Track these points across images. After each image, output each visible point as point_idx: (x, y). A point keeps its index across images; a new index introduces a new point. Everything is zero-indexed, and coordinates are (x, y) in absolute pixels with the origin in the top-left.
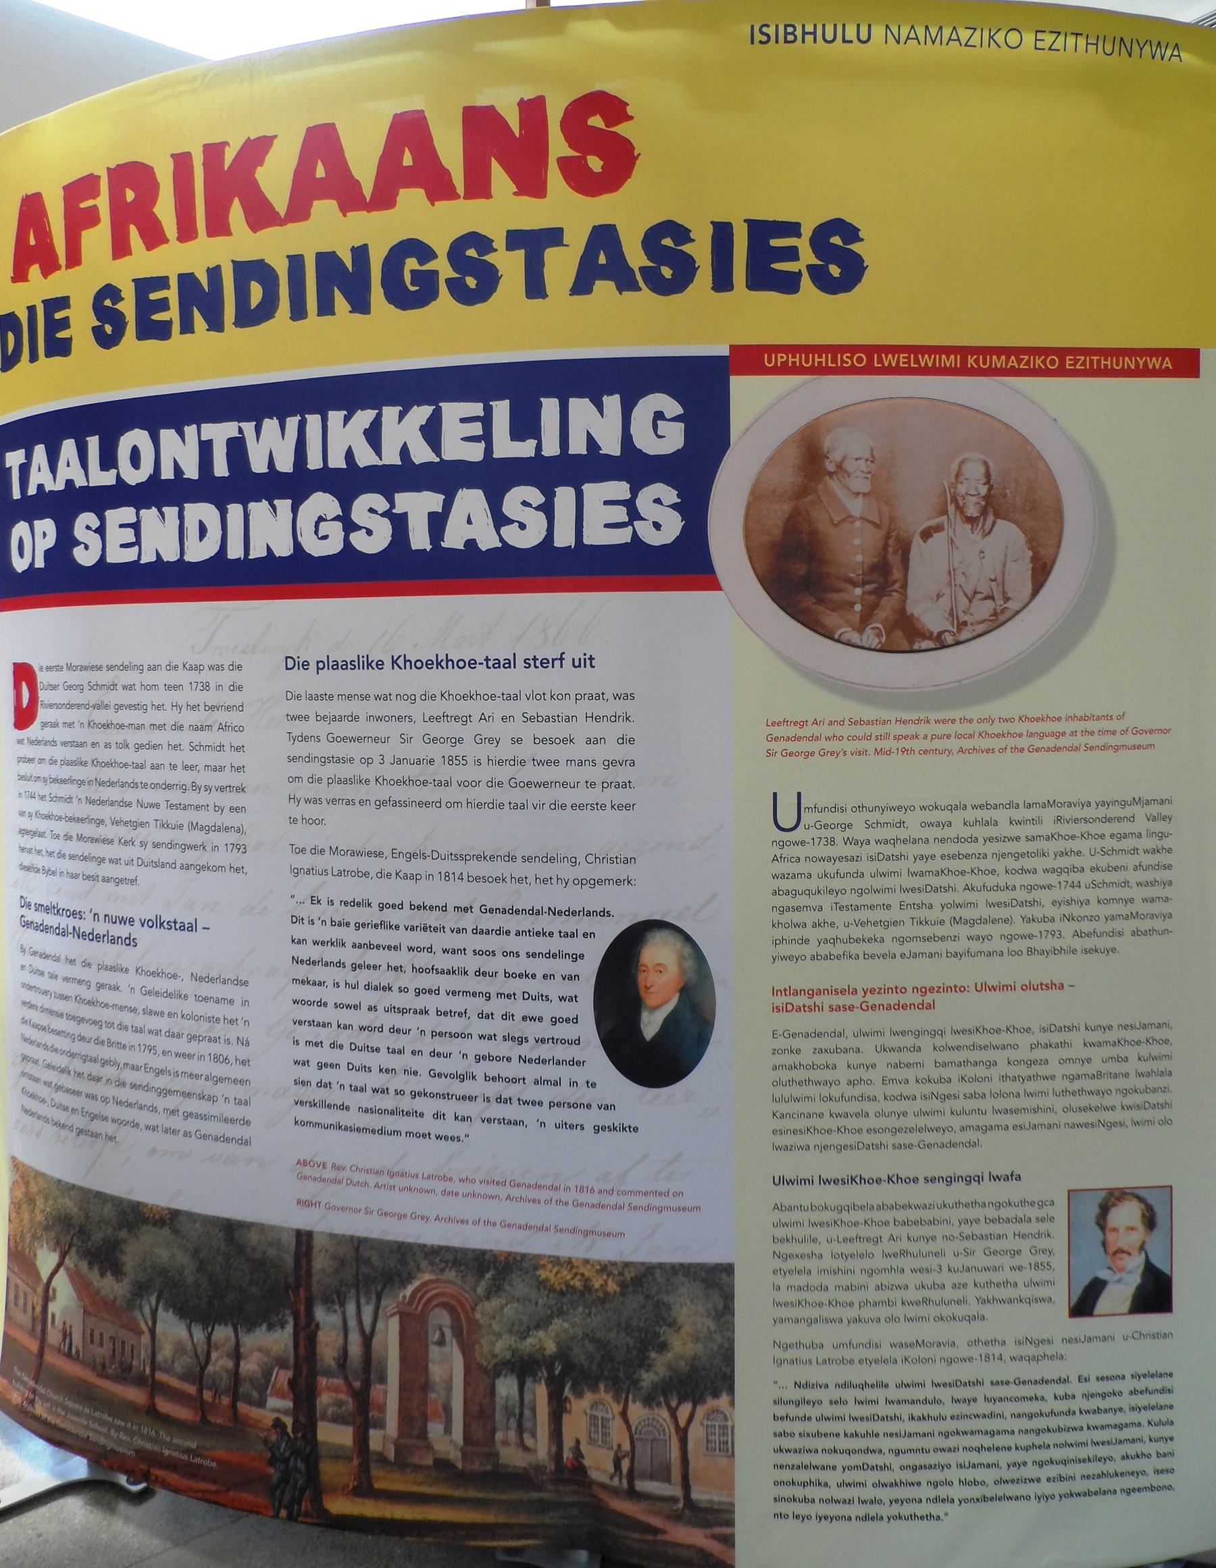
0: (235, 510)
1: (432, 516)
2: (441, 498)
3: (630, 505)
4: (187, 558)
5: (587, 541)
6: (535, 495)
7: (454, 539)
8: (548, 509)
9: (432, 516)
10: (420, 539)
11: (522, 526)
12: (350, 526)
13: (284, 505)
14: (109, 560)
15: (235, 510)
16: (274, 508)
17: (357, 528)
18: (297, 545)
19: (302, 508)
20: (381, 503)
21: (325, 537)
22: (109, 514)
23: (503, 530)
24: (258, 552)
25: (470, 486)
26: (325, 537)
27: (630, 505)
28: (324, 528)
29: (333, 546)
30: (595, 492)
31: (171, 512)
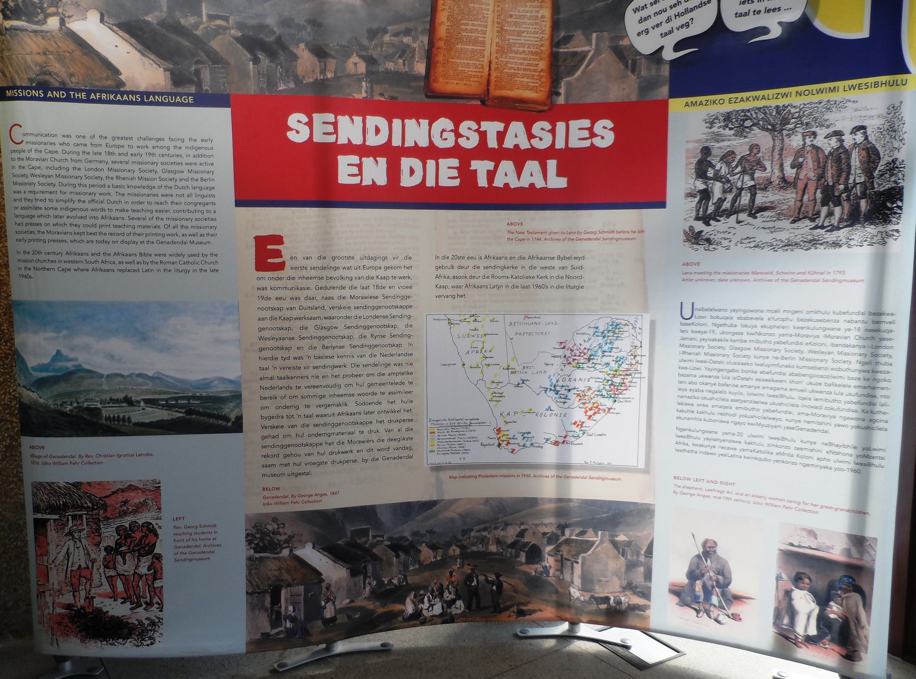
0: (397, 123)
1: (489, 171)
2: (493, 164)
3: (591, 129)
4: (367, 144)
5: (570, 146)
6: (547, 125)
7: (499, 182)
8: (553, 131)
9: (489, 171)
10: (492, 143)
11: (298, 132)
12: (458, 135)
13: (425, 123)
14: (315, 140)
15: (397, 123)
16: (419, 123)
17: (462, 136)
18: (431, 142)
19: (434, 125)
20: (474, 125)
21: (446, 139)
22: (315, 116)
23: (532, 140)
24: (409, 143)
25: (517, 120)
26: (446, 139)
27: (591, 129)
28: (445, 135)
29: (450, 143)
30: (574, 124)
31: (358, 120)
